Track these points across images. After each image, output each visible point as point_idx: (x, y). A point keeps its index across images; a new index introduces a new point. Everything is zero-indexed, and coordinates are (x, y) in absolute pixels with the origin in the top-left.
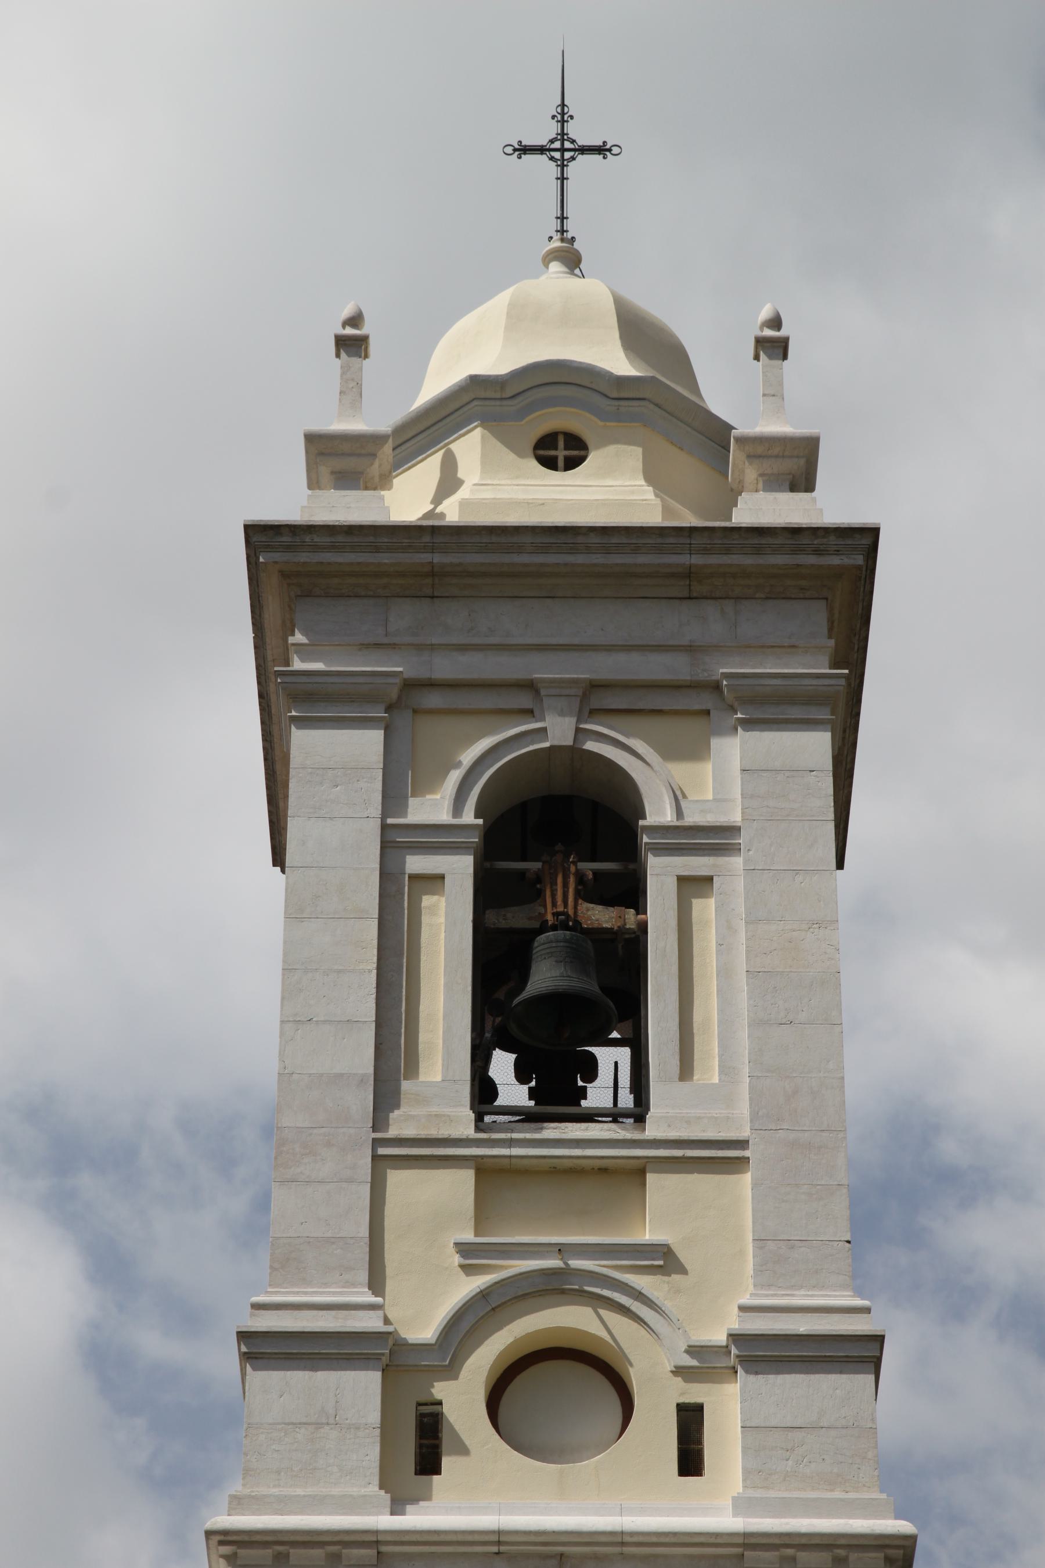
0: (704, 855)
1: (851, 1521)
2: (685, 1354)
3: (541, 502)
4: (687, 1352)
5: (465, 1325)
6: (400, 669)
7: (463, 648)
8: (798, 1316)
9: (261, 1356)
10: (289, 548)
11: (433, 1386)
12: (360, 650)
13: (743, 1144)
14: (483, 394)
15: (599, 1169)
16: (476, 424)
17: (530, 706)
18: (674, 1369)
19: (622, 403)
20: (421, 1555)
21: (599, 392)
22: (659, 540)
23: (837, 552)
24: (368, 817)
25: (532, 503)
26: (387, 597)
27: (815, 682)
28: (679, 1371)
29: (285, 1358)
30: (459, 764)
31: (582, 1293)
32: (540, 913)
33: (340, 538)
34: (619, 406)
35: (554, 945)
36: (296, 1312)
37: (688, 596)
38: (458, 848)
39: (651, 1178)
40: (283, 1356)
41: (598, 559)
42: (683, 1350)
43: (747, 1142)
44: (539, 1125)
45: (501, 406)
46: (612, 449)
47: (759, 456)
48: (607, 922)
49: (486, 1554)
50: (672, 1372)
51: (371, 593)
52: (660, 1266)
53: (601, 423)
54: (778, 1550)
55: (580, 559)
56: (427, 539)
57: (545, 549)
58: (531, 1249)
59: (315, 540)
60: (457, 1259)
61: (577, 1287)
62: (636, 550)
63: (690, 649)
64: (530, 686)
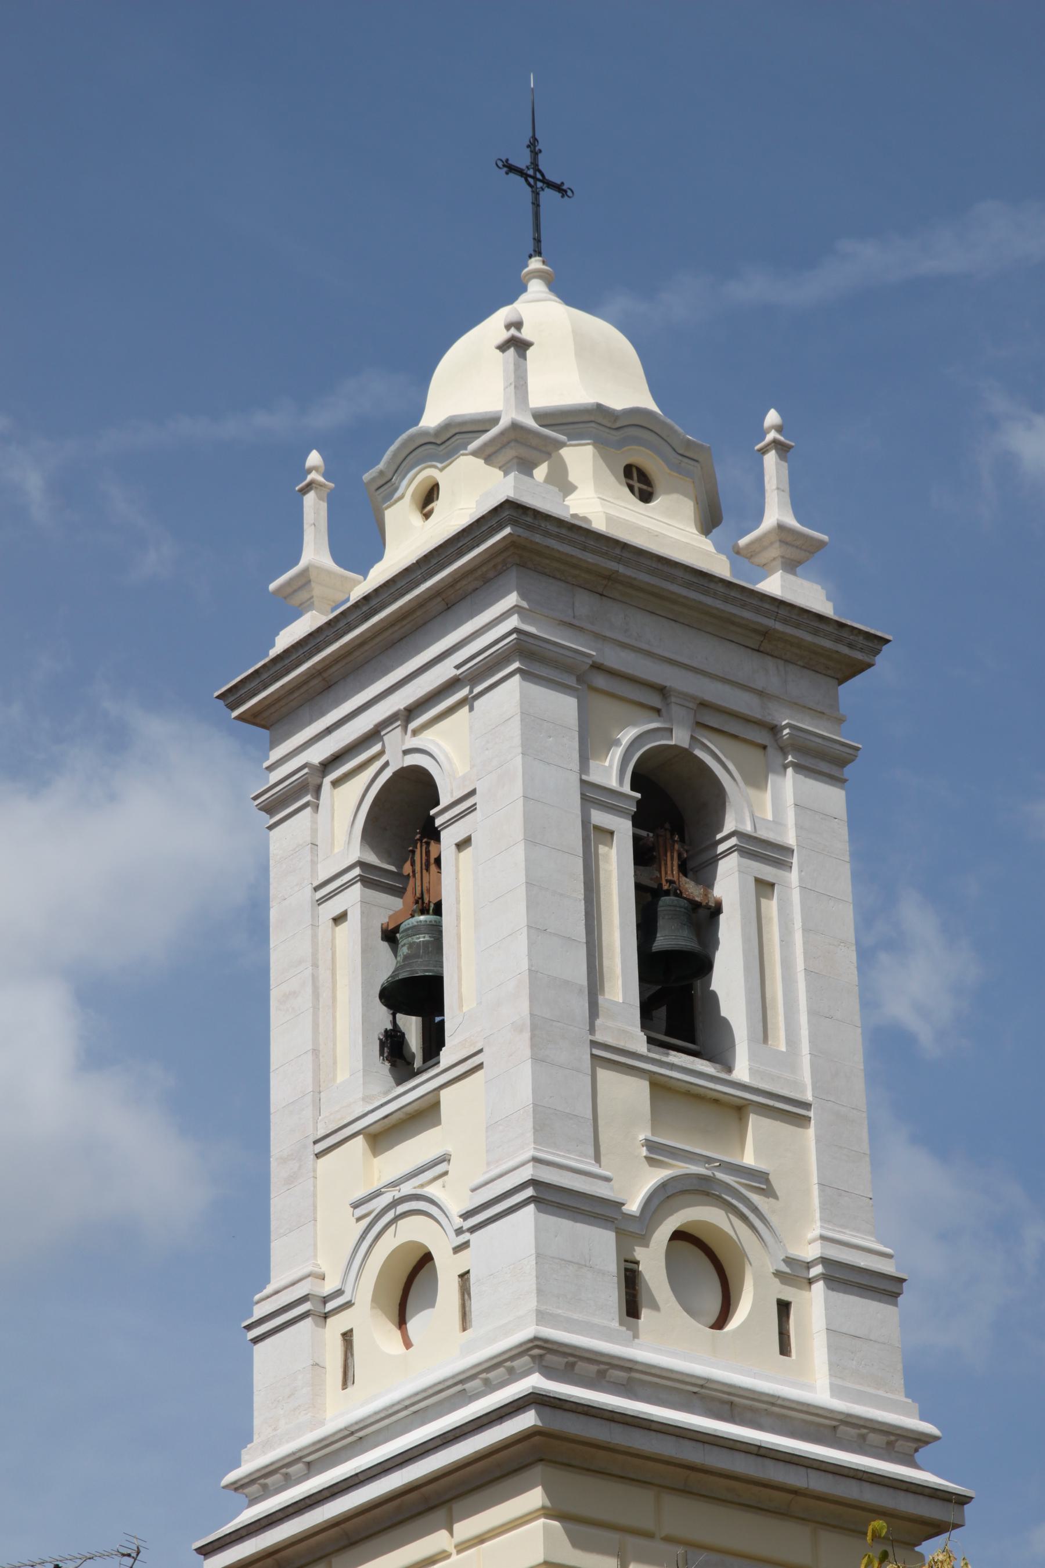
0: (769, 865)
1: (855, 1406)
2: (782, 1262)
3: (656, 534)
4: (784, 1260)
7: (624, 646)
9: (543, 1201)
10: (529, 527)
11: (634, 1250)
12: (559, 624)
13: (807, 1106)
14: (600, 420)
15: (714, 1099)
16: (589, 441)
18: (775, 1272)
21: (671, 446)
22: (760, 604)
23: (861, 650)
24: (571, 770)
25: (651, 533)
26: (573, 584)
28: (778, 1274)
29: (557, 1207)
30: (617, 743)
31: (719, 1198)
32: (657, 877)
33: (564, 531)
34: (681, 461)
37: (757, 648)
38: (622, 812)
39: (753, 1120)
40: (556, 1205)
41: (719, 604)
42: (782, 1258)
44: (665, 1050)
46: (675, 496)
48: (698, 897)
50: (773, 1273)
51: (563, 578)
52: (763, 1189)
53: (669, 471)
54: (859, 1429)
55: (709, 601)
56: (618, 551)
57: (688, 585)
59: (548, 527)
60: (644, 1152)
61: (718, 1193)
62: (744, 605)
63: (761, 694)
64: (662, 691)
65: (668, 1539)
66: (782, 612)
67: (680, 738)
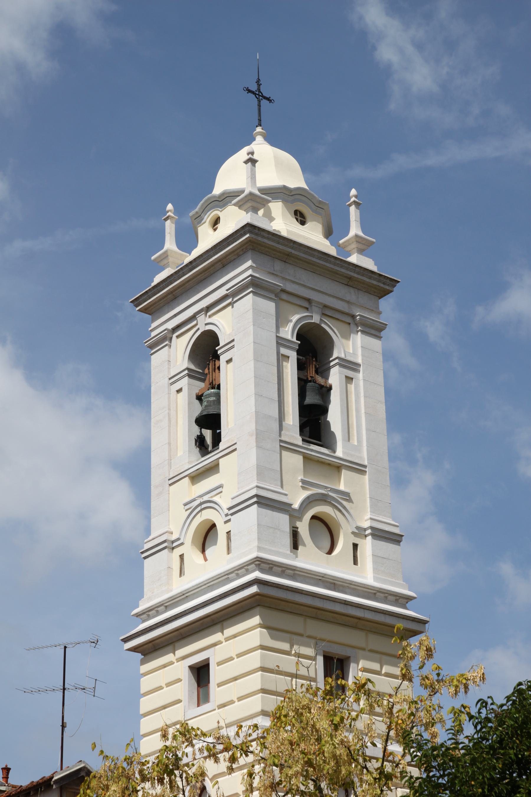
3: (307, 238)
4: (355, 528)
5: (304, 506)
6: (282, 285)
7: (294, 282)
8: (276, 494)
10: (257, 234)
12: (268, 273)
13: (365, 466)
17: (308, 307)
19: (319, 208)
20: (302, 576)
22: (348, 266)
23: (388, 285)
27: (371, 321)
28: (353, 533)
30: (291, 321)
31: (330, 503)
33: (270, 236)
35: (314, 388)
36: (267, 491)
39: (344, 472)
41: (332, 266)
43: (366, 466)
45: (288, 197)
46: (315, 223)
47: (359, 242)
49: (317, 579)
50: (351, 533)
52: (347, 499)
55: (328, 265)
56: (292, 244)
57: (320, 258)
58: (319, 486)
60: (300, 484)
62: (342, 267)
63: (348, 302)
64: (309, 301)
65: (309, 637)
66: (357, 269)
67: (316, 319)
